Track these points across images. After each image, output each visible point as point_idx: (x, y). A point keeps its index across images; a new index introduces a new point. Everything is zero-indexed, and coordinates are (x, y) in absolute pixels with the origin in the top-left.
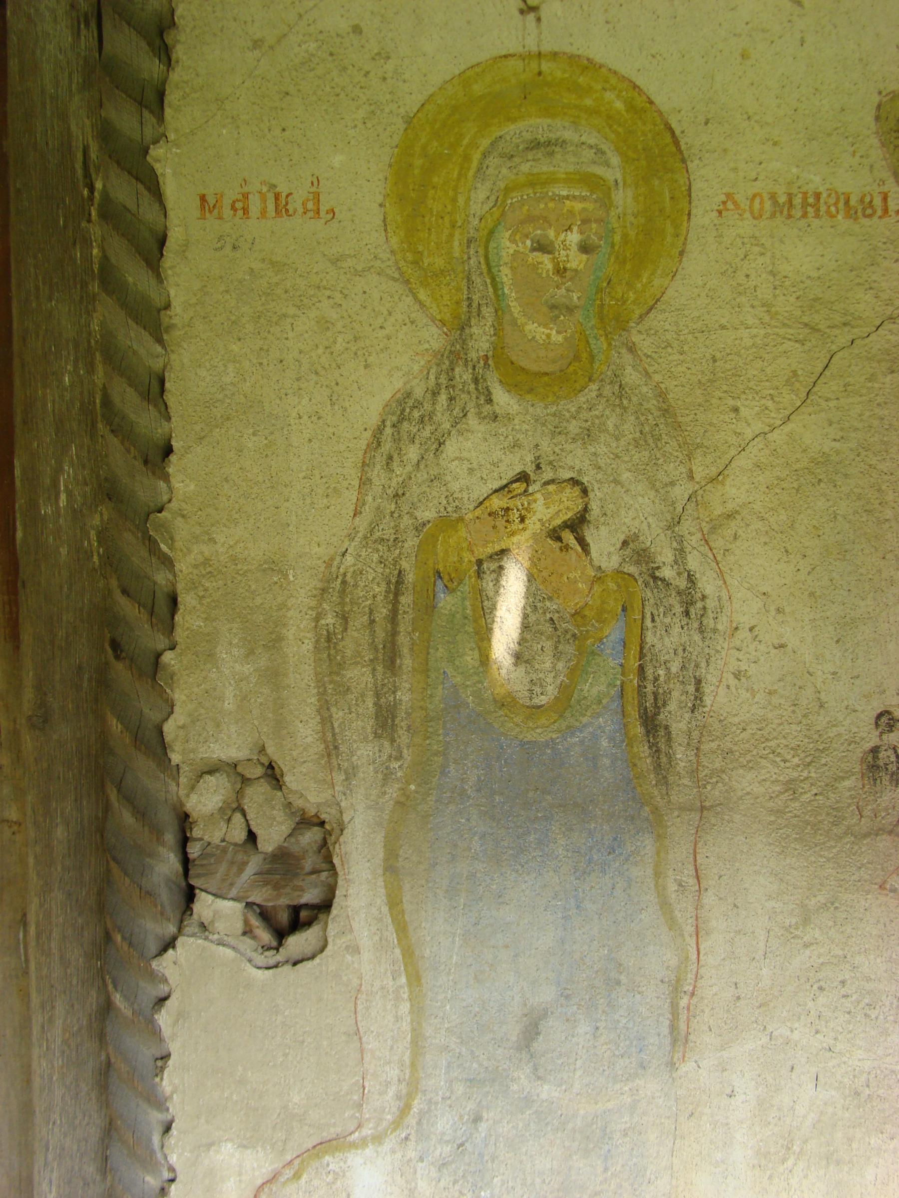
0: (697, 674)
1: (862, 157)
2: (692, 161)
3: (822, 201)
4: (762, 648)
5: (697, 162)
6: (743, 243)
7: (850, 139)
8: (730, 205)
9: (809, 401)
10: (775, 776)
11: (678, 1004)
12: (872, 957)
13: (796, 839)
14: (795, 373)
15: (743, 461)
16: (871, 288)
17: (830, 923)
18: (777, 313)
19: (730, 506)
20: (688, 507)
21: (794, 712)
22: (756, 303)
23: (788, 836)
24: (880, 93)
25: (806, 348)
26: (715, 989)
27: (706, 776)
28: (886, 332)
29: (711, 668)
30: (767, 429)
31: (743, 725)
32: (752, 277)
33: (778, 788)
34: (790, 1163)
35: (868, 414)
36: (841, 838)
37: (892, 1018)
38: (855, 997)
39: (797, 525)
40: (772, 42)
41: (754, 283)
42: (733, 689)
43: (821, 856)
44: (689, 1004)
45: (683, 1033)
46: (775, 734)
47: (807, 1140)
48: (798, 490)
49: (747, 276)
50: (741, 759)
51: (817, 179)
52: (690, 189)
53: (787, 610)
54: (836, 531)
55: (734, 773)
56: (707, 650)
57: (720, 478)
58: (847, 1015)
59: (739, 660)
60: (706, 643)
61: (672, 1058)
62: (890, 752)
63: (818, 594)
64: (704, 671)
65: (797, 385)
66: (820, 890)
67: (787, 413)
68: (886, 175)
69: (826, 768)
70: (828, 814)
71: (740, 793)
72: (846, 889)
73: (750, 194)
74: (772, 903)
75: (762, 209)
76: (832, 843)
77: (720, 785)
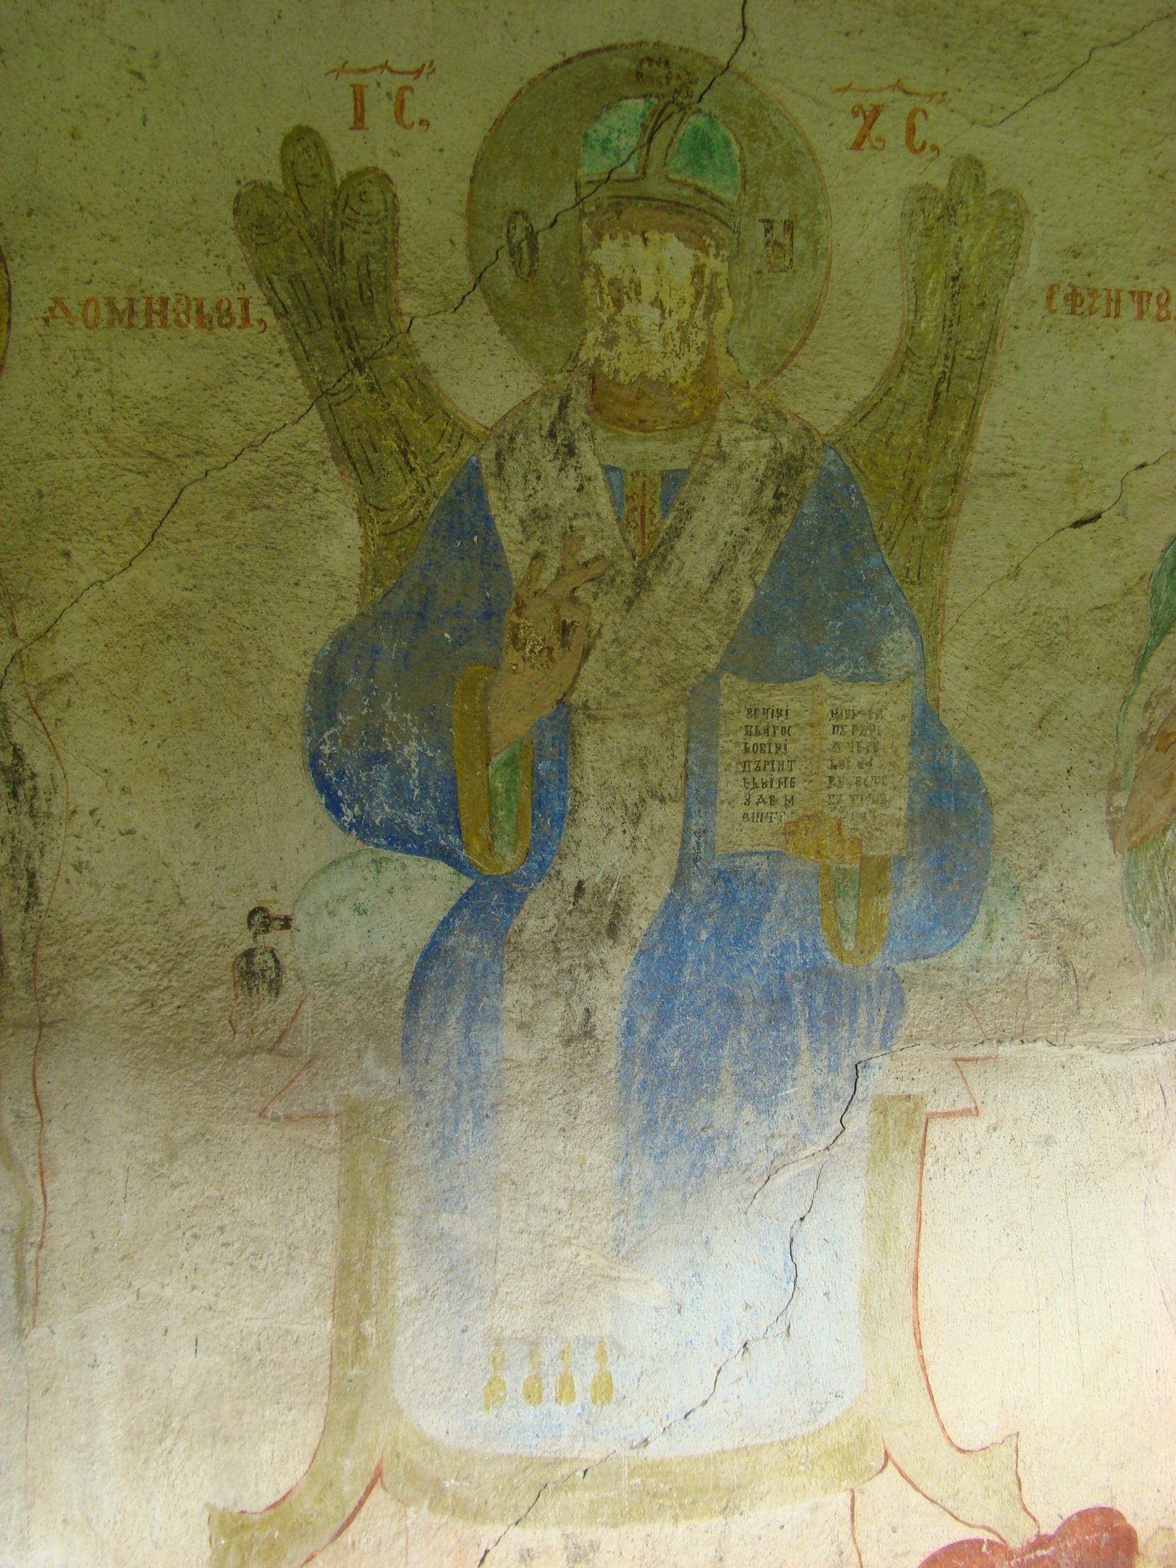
0: (30, 866)
1: (217, 256)
2: (12, 260)
3: (170, 307)
4: (106, 834)
5: (18, 260)
6: (75, 357)
7: (204, 236)
8: (59, 312)
9: (154, 543)
10: (128, 986)
11: (23, 1258)
12: (254, 1198)
13: (155, 1060)
14: (137, 511)
15: (76, 615)
16: (229, 410)
17: (202, 1159)
18: (115, 440)
19: (62, 668)
20: (11, 669)
21: (148, 910)
22: (89, 428)
23: (146, 1057)
24: (238, 182)
25: (151, 481)
26: (67, 1240)
27: (45, 986)
28: (247, 462)
29: (47, 856)
30: (104, 577)
31: (88, 926)
32: (86, 397)
33: (133, 1000)
34: (168, 1443)
35: (225, 558)
36: (211, 1058)
37: (283, 1269)
38: (236, 1245)
39: (142, 690)
40: (108, 120)
41: (88, 404)
42: (73, 883)
43: (187, 1080)
44: (38, 1257)
45: (32, 1292)
46: (127, 936)
47: (188, 1416)
48: (142, 649)
49: (80, 396)
50: (86, 967)
51: (164, 282)
52: (9, 294)
53: (134, 789)
54: (190, 697)
55: (78, 983)
56: (40, 838)
57: (49, 634)
58: (229, 1268)
59: (79, 849)
60: (39, 830)
61: (21, 1322)
62: (267, 956)
63: (171, 770)
64: (37, 863)
65: (141, 524)
66: (187, 1120)
67: (128, 557)
68: (247, 277)
69: (189, 976)
70: (194, 1030)
71: (86, 1007)
72: (218, 1118)
73: (83, 299)
74: (129, 1137)
75: (97, 317)
76: (200, 1064)
77: (62, 997)
